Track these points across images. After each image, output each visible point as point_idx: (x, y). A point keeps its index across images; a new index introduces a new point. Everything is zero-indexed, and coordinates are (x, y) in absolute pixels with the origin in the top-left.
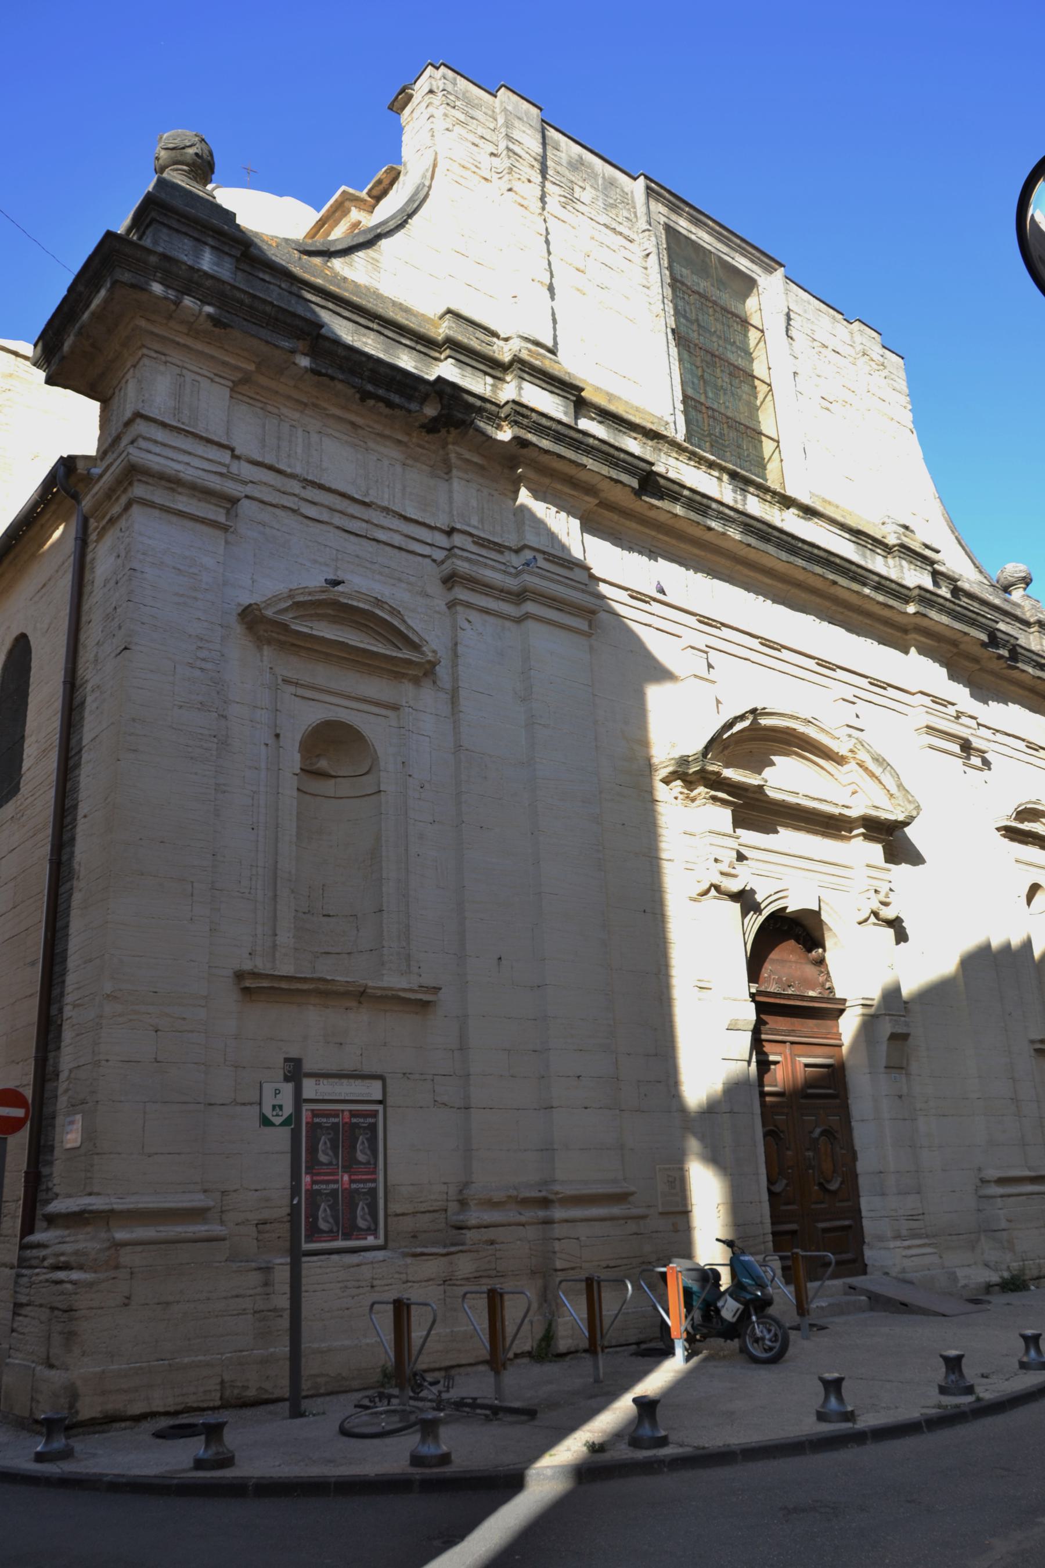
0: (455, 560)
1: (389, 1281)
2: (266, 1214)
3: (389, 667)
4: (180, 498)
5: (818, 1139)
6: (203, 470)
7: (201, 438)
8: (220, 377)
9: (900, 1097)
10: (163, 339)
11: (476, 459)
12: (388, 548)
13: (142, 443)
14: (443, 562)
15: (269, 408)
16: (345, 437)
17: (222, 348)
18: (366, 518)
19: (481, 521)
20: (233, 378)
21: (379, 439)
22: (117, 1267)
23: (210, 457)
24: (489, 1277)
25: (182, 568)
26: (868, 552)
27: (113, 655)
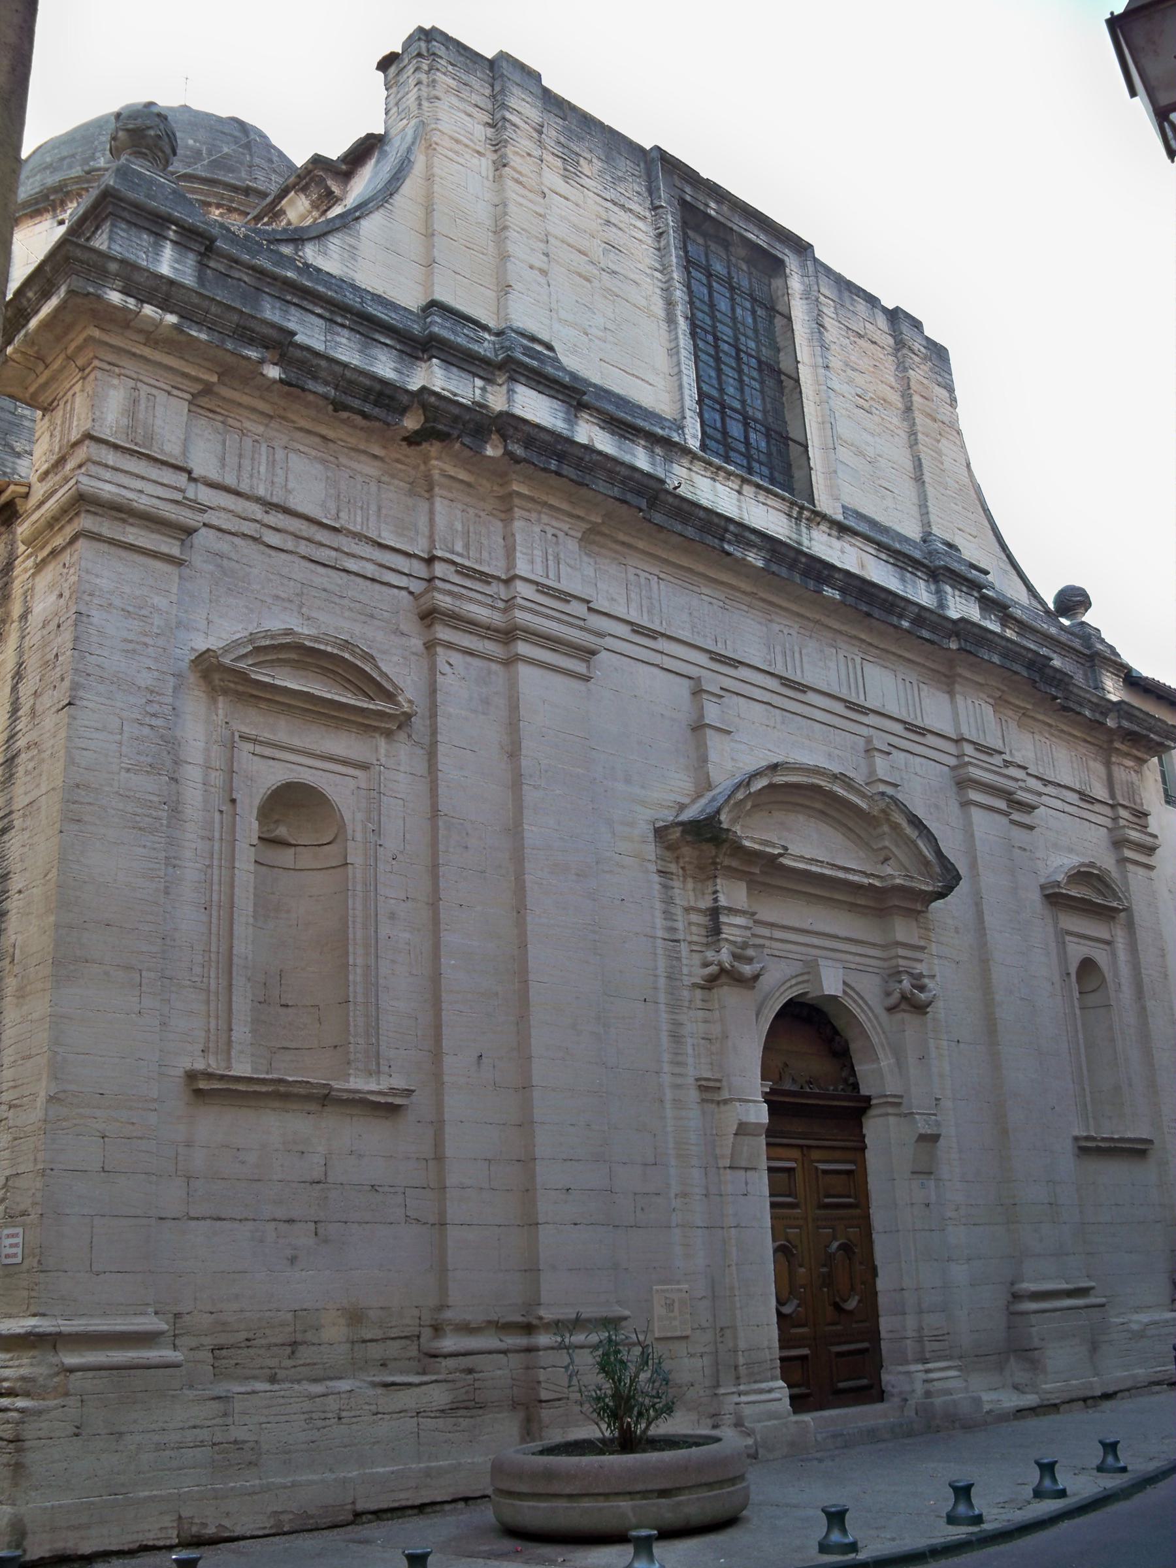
0: (436, 594)
1: (358, 1413)
2: (222, 1339)
3: (360, 720)
4: (129, 529)
5: (834, 1254)
6: (158, 498)
7: (156, 460)
8: (179, 389)
9: (928, 1205)
10: (119, 350)
11: (463, 475)
12: (359, 580)
13: (94, 469)
14: (421, 595)
15: (230, 421)
16: (314, 453)
17: (182, 358)
18: (335, 545)
19: (467, 546)
20: (192, 390)
21: (353, 454)
22: (67, 1394)
23: (165, 482)
24: (466, 1408)
25: (131, 609)
26: (908, 575)
27: (54, 709)
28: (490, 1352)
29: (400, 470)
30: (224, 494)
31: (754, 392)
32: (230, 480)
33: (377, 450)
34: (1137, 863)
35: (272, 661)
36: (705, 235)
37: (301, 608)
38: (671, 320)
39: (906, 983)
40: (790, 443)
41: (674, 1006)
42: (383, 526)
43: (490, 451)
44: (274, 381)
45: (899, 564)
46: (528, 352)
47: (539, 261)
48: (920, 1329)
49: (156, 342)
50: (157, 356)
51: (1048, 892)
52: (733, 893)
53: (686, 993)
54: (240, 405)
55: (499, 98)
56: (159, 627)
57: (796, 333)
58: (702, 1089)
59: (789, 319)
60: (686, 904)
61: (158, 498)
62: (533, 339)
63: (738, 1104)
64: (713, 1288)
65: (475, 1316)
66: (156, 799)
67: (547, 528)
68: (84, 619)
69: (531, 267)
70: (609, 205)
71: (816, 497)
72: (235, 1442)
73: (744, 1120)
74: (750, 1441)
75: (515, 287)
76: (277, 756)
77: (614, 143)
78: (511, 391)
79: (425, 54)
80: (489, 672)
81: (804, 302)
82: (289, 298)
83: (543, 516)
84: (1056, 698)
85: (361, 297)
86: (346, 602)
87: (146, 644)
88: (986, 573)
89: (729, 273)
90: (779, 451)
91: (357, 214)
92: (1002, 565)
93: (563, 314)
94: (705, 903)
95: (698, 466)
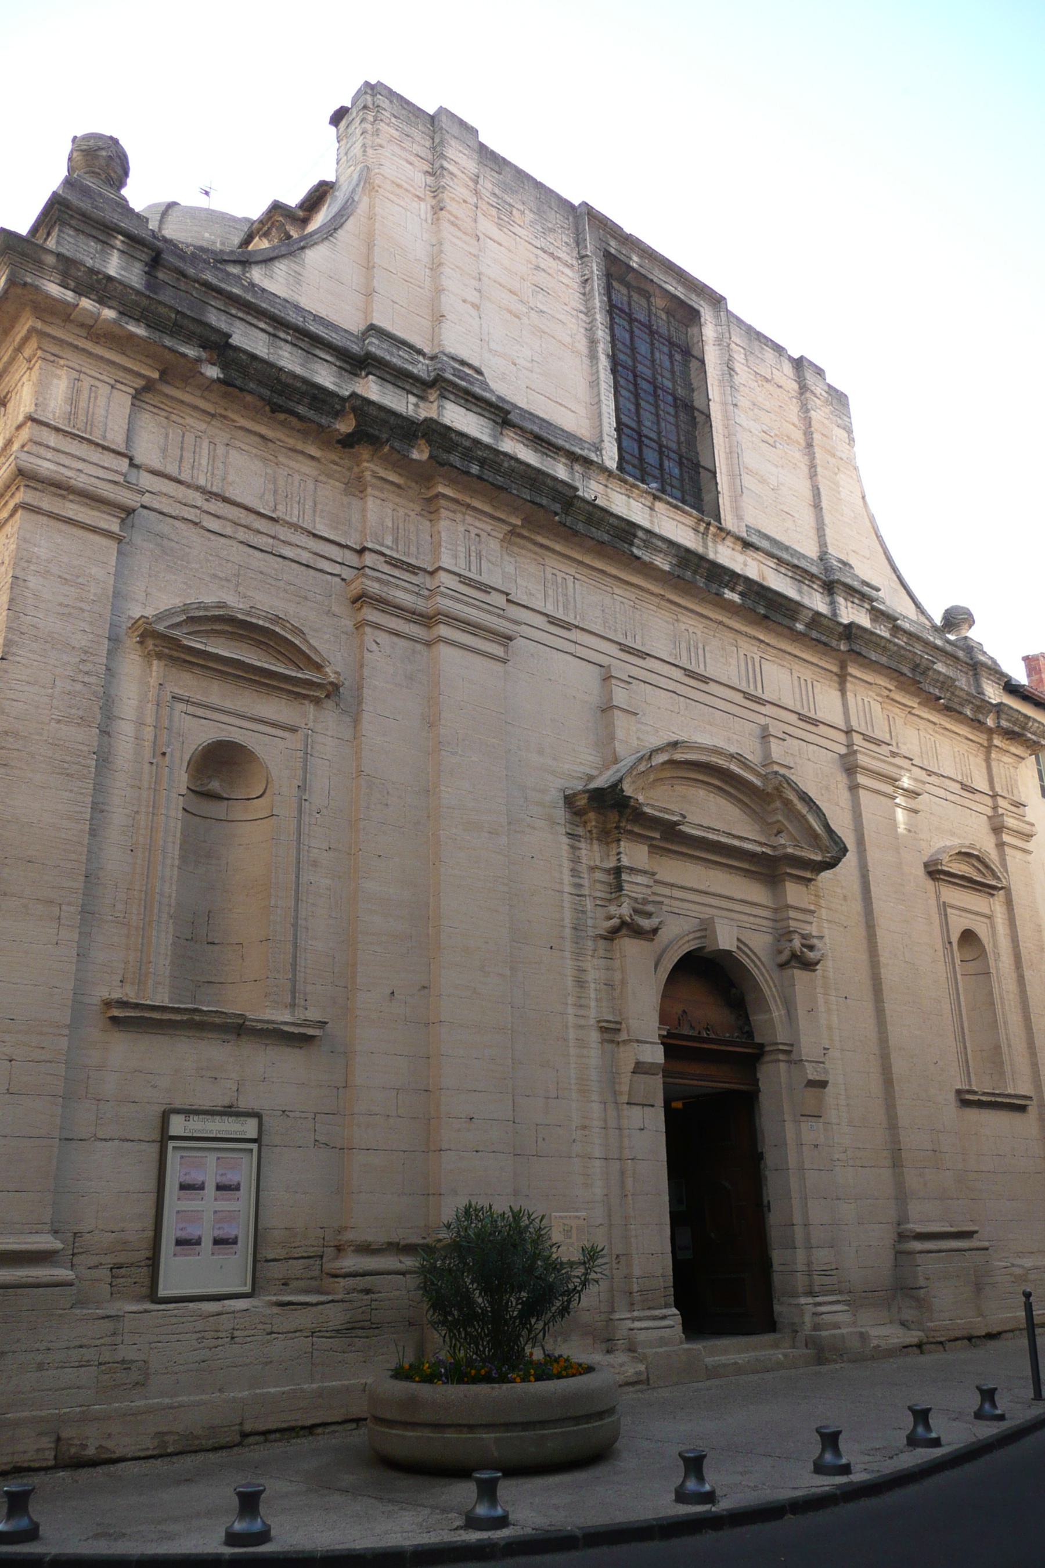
3: (290, 688)
6: (98, 478)
9: (816, 1146)
10: (61, 342)
12: (294, 565)
16: (254, 451)
19: (396, 541)
21: (290, 454)
23: (106, 465)
25: (68, 577)
26: (805, 587)
28: (389, 1273)
29: (335, 471)
30: (166, 481)
31: (668, 426)
32: (172, 469)
33: (313, 451)
34: (1016, 847)
35: (206, 631)
36: (628, 286)
37: (237, 586)
38: (593, 356)
39: (797, 943)
40: (701, 470)
41: (578, 955)
42: (318, 519)
43: (415, 455)
44: (213, 381)
45: (798, 577)
46: (457, 373)
47: (473, 296)
48: (809, 1264)
49: (98, 336)
50: (99, 350)
51: (931, 869)
52: (634, 854)
53: (590, 943)
54: (182, 402)
55: (438, 149)
56: (95, 594)
57: (709, 374)
58: (603, 1030)
59: (703, 362)
60: (592, 864)
61: (98, 478)
62: (463, 363)
63: (635, 1045)
64: (610, 1216)
65: (377, 1236)
66: (86, 748)
67: (471, 528)
68: (20, 583)
69: (464, 301)
70: (539, 252)
71: (722, 516)
72: (123, 1362)
73: (642, 1059)
74: (642, 1368)
75: (448, 317)
76: (209, 717)
77: (545, 197)
78: (441, 407)
79: (370, 109)
80: (414, 652)
81: (717, 348)
82: (234, 312)
83: (467, 517)
84: (940, 698)
85: (304, 318)
86: (281, 584)
87: (82, 610)
88: (878, 590)
89: (649, 321)
90: (691, 478)
91: (302, 244)
92: (893, 585)
93: (493, 346)
94: (612, 863)
95: (614, 484)
